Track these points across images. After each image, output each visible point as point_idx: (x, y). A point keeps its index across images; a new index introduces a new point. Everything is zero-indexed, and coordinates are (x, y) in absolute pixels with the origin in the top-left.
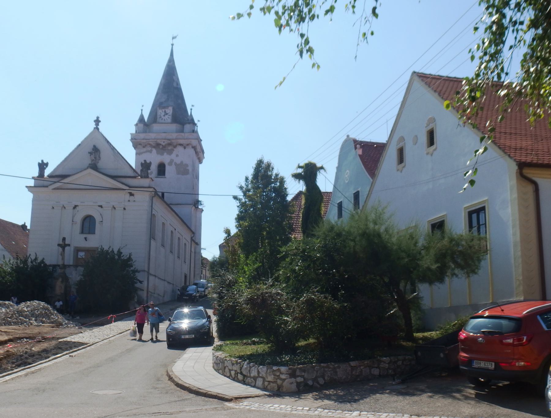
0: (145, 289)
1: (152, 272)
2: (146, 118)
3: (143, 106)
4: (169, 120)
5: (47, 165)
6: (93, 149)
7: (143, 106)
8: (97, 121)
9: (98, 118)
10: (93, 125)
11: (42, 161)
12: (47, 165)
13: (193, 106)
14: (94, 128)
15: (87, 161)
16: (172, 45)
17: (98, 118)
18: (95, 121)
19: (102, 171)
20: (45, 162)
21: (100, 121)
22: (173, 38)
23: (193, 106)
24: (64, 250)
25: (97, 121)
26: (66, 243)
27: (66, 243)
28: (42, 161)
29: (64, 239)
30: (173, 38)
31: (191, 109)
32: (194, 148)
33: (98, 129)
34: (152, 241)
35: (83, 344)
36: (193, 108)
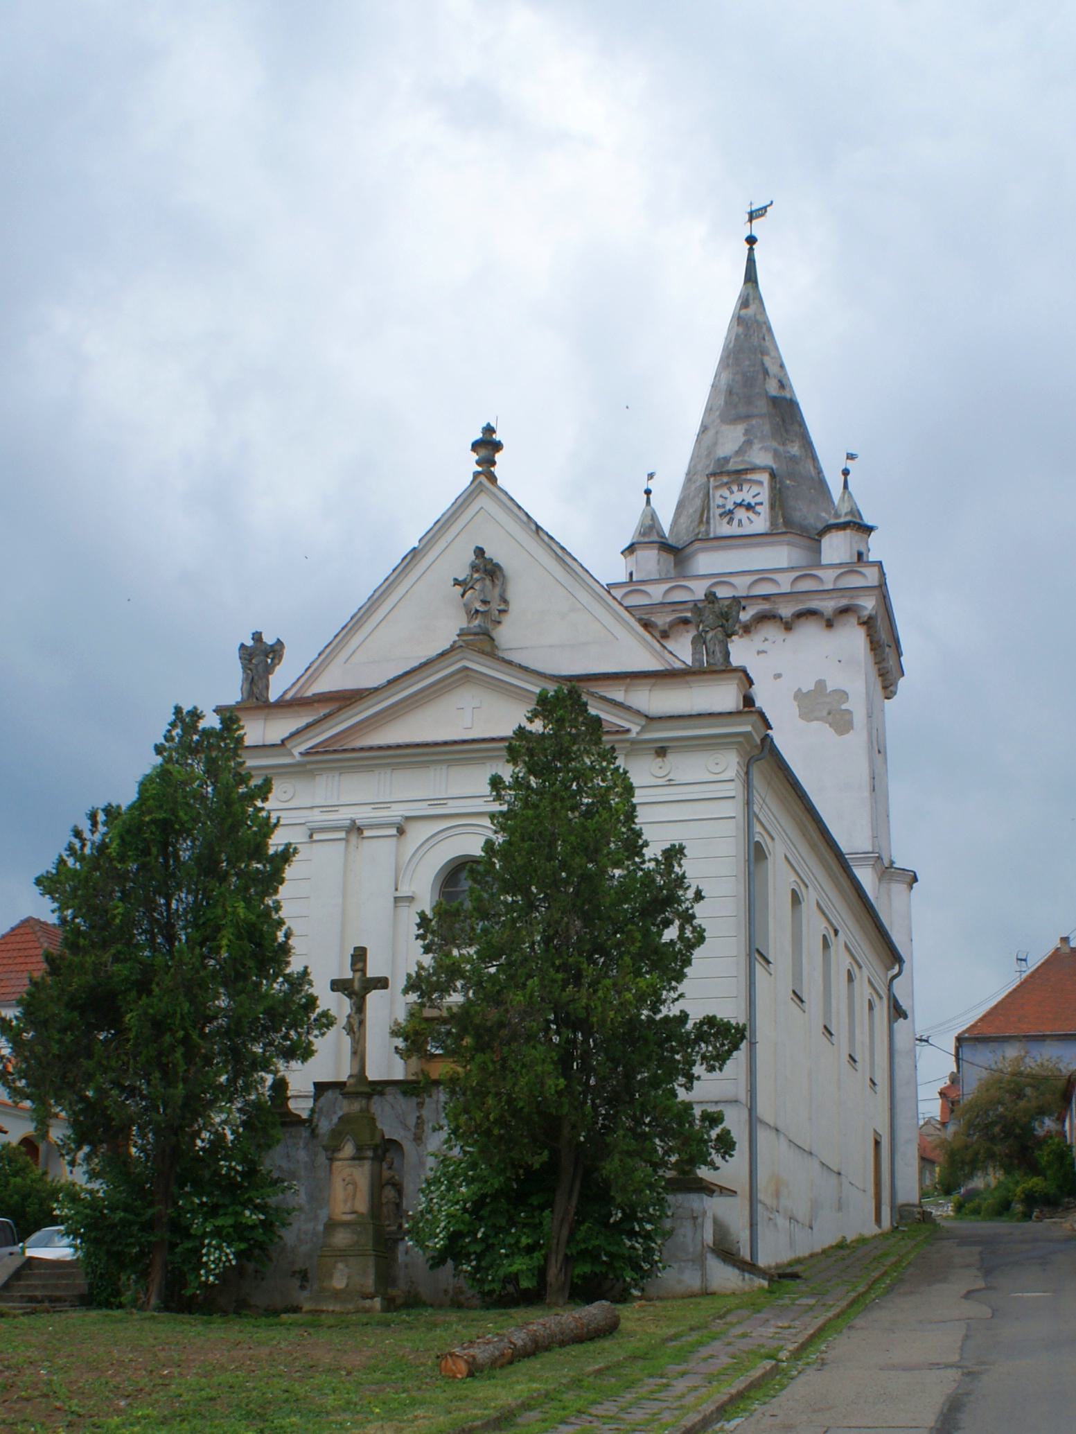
0: (742, 1185)
1: (763, 1110)
2: (666, 520)
3: (651, 476)
4: (760, 523)
5: (275, 652)
6: (475, 568)
7: (651, 476)
8: (487, 446)
9: (489, 430)
10: (469, 463)
11: (257, 637)
12: (275, 652)
13: (851, 457)
14: (476, 475)
15: (447, 627)
16: (751, 240)
17: (489, 430)
18: (476, 446)
19: (516, 657)
20: (269, 639)
21: (497, 446)
22: (752, 216)
23: (851, 457)
24: (360, 1008)
25: (487, 446)
26: (371, 973)
27: (371, 973)
28: (257, 637)
29: (360, 956)
30: (752, 216)
31: (846, 473)
32: (868, 623)
33: (492, 478)
34: (759, 968)
35: (722, 1189)
36: (850, 465)
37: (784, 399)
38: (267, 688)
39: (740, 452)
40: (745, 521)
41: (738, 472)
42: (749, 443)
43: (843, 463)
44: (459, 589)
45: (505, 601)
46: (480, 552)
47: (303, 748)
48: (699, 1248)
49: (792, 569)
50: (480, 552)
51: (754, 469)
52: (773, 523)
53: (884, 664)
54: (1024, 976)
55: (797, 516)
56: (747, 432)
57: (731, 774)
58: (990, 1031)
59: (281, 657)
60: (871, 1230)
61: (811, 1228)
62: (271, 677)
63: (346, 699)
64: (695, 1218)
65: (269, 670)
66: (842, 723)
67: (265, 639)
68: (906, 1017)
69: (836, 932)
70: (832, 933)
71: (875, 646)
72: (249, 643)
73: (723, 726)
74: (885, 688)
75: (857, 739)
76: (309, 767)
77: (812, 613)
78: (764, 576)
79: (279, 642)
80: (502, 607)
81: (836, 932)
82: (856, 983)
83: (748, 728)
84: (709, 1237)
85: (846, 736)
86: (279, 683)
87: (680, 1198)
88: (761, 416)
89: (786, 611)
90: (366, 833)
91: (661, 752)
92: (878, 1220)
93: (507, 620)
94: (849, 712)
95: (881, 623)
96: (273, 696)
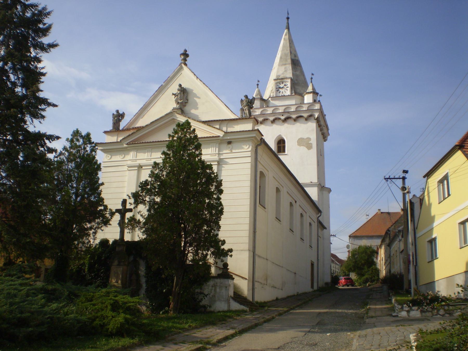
4: (288, 93)
6: (179, 90)
9: (186, 51)
11: (117, 111)
17: (186, 51)
28: (117, 111)
32: (318, 120)
34: (259, 208)
36: (313, 76)
37: (295, 59)
38: (119, 126)
39: (283, 74)
40: (284, 92)
41: (282, 79)
42: (286, 71)
43: (311, 76)
44: (174, 96)
45: (187, 100)
46: (180, 85)
47: (126, 143)
48: (227, 297)
49: (296, 104)
50: (180, 85)
51: (286, 78)
52: (291, 93)
53: (323, 132)
54: (368, 220)
55: (298, 91)
56: (285, 68)
57: (250, 149)
58: (358, 235)
59: (124, 117)
60: (309, 289)
61: (282, 290)
62: (120, 123)
63: (139, 129)
64: (226, 287)
65: (120, 121)
66: (309, 147)
67: (120, 112)
68: (326, 228)
69: (296, 202)
70: (294, 202)
71: (319, 125)
72: (115, 113)
73: (248, 134)
74: (324, 138)
75: (314, 151)
76: (128, 148)
77: (301, 117)
78: (288, 107)
79: (124, 113)
80: (186, 101)
81: (296, 202)
82: (304, 217)
83: (254, 135)
84: (231, 293)
85: (278, 135)
86: (123, 125)
87: (222, 280)
88: (289, 64)
89: (294, 116)
90: (143, 168)
91: (229, 143)
92: (312, 286)
93: (188, 105)
94: (311, 144)
95: (321, 119)
96: (121, 128)
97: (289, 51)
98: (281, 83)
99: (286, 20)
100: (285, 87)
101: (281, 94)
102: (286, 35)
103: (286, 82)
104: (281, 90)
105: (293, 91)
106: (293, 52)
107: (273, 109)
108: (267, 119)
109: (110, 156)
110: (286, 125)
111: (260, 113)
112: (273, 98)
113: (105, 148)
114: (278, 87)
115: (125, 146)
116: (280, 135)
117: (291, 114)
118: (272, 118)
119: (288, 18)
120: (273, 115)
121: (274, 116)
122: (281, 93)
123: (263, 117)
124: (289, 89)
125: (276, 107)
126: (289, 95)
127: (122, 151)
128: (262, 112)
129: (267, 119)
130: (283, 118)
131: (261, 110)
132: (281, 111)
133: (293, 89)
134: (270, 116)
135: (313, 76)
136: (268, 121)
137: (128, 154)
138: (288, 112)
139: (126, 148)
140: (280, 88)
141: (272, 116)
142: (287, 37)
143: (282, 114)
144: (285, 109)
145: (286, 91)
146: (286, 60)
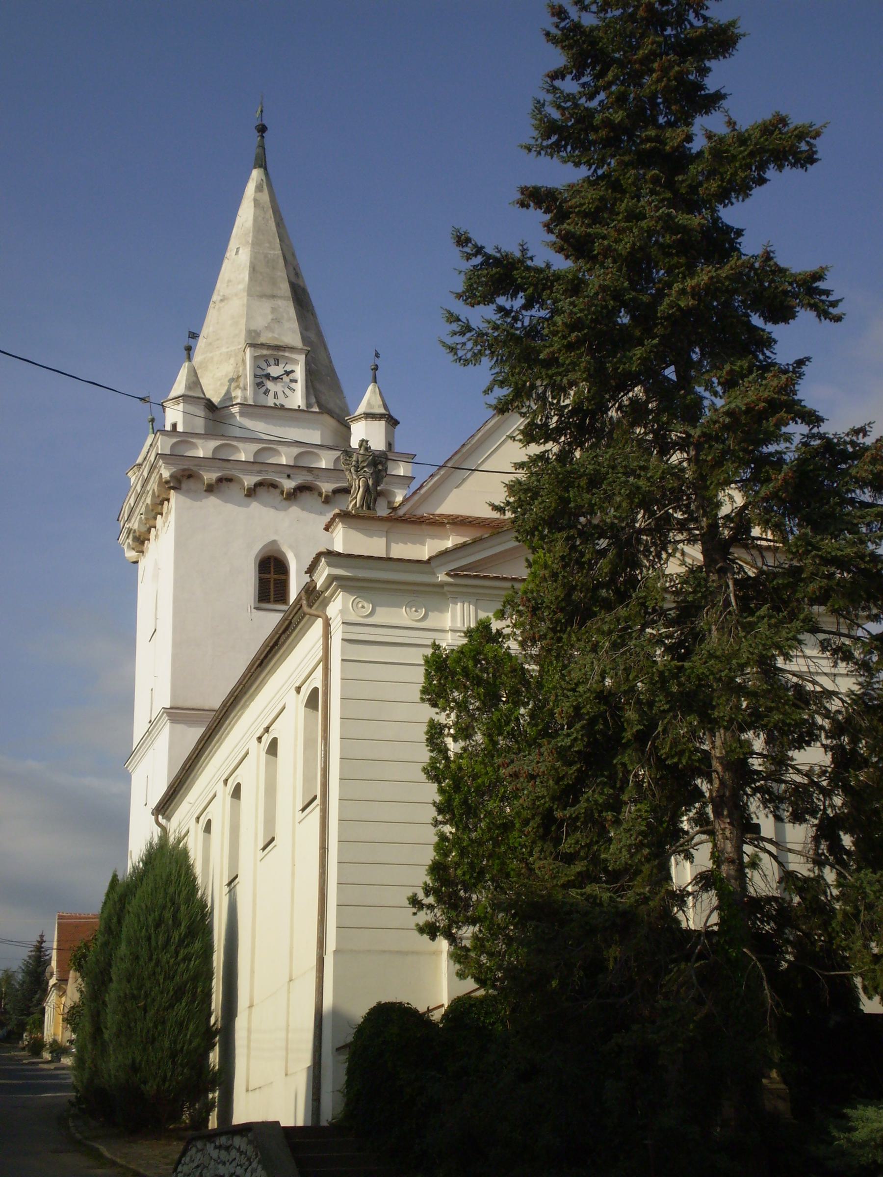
4: (297, 399)
39: (268, 328)
40: (280, 394)
41: (278, 348)
42: (277, 320)
52: (309, 405)
97: (279, 252)
98: (272, 362)
99: (256, 137)
100: (286, 379)
101: (271, 401)
102: (259, 189)
103: (289, 361)
104: (270, 385)
105: (313, 400)
106: (289, 257)
107: (256, 447)
108: (229, 480)
109: (369, 607)
110: (295, 511)
111: (209, 454)
112: (250, 409)
113: (361, 574)
114: (260, 372)
115: (442, 577)
116: (274, 542)
117: (317, 477)
118: (249, 481)
119: (262, 129)
120: (257, 467)
121: (260, 472)
122: (271, 394)
123: (220, 469)
124: (299, 387)
125: (270, 446)
126: (299, 410)
127: (414, 592)
128: (216, 449)
129: (229, 480)
130: (289, 485)
131: (213, 444)
132: (284, 461)
133: (311, 391)
134: (244, 471)
135: (378, 361)
136: (231, 485)
137: (442, 610)
138: (310, 470)
139: (442, 585)
140: (268, 376)
141: (251, 473)
142: (265, 197)
143: (289, 471)
144: (298, 457)
145: (287, 391)
146: (274, 282)
